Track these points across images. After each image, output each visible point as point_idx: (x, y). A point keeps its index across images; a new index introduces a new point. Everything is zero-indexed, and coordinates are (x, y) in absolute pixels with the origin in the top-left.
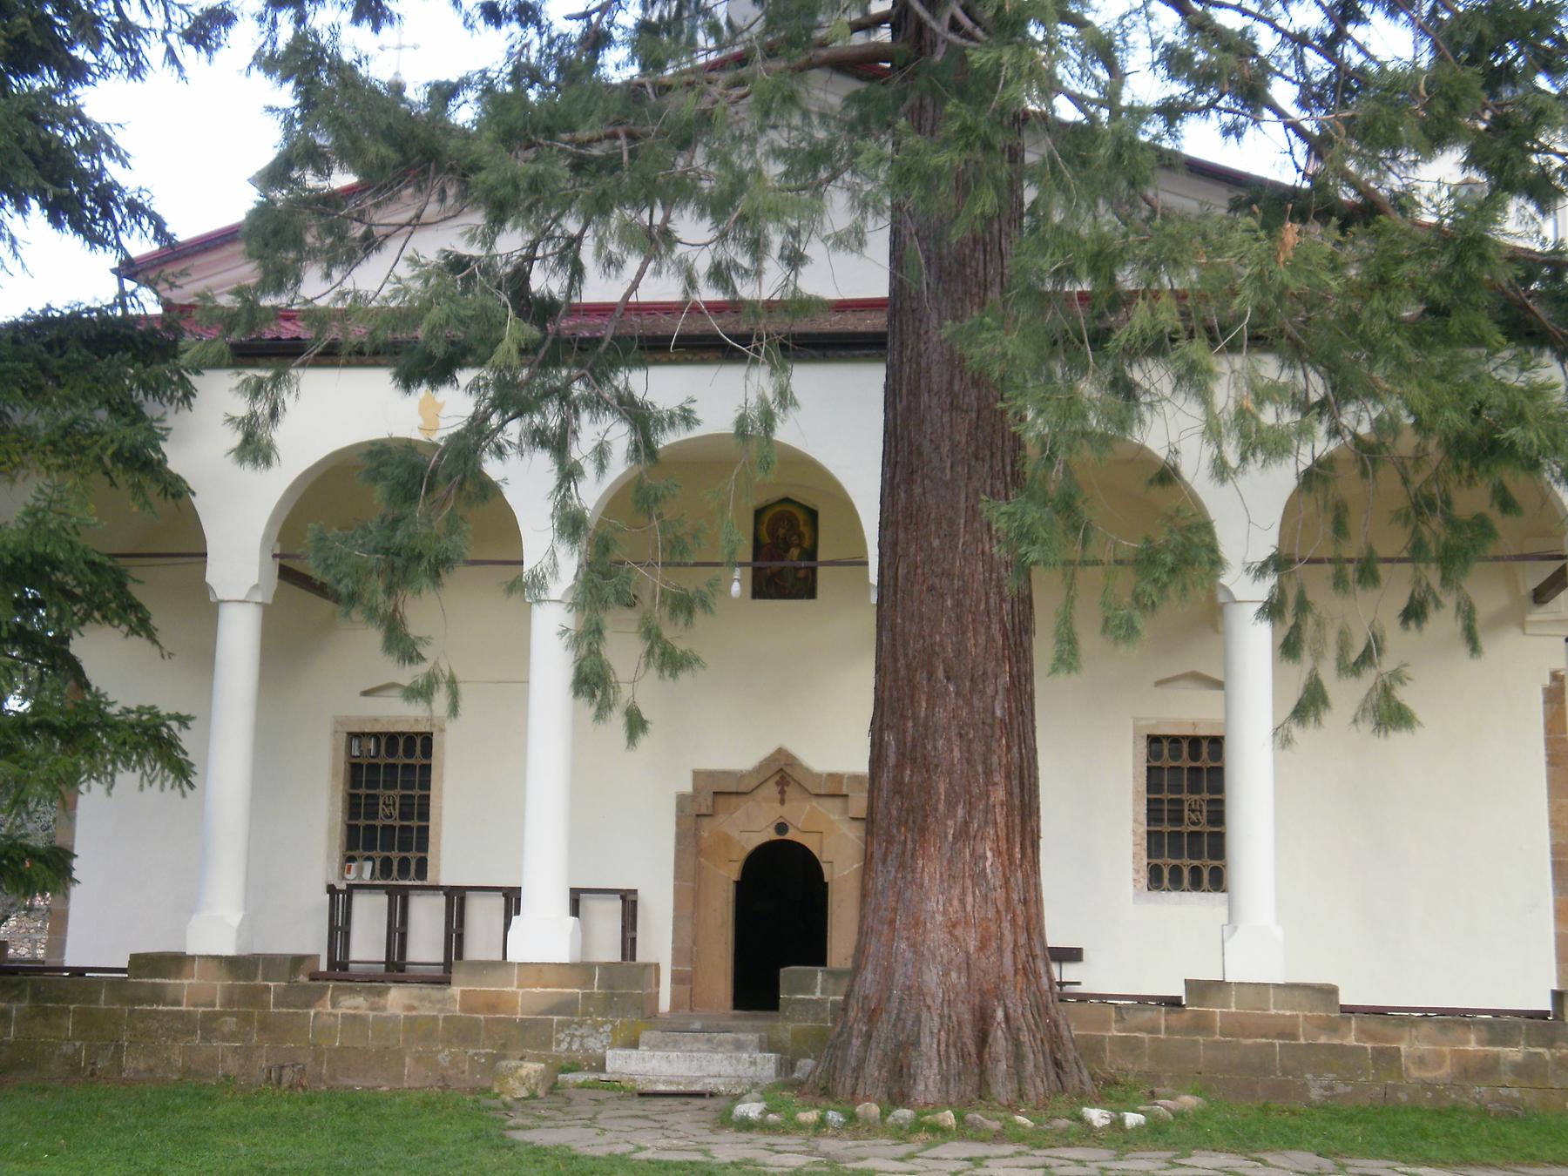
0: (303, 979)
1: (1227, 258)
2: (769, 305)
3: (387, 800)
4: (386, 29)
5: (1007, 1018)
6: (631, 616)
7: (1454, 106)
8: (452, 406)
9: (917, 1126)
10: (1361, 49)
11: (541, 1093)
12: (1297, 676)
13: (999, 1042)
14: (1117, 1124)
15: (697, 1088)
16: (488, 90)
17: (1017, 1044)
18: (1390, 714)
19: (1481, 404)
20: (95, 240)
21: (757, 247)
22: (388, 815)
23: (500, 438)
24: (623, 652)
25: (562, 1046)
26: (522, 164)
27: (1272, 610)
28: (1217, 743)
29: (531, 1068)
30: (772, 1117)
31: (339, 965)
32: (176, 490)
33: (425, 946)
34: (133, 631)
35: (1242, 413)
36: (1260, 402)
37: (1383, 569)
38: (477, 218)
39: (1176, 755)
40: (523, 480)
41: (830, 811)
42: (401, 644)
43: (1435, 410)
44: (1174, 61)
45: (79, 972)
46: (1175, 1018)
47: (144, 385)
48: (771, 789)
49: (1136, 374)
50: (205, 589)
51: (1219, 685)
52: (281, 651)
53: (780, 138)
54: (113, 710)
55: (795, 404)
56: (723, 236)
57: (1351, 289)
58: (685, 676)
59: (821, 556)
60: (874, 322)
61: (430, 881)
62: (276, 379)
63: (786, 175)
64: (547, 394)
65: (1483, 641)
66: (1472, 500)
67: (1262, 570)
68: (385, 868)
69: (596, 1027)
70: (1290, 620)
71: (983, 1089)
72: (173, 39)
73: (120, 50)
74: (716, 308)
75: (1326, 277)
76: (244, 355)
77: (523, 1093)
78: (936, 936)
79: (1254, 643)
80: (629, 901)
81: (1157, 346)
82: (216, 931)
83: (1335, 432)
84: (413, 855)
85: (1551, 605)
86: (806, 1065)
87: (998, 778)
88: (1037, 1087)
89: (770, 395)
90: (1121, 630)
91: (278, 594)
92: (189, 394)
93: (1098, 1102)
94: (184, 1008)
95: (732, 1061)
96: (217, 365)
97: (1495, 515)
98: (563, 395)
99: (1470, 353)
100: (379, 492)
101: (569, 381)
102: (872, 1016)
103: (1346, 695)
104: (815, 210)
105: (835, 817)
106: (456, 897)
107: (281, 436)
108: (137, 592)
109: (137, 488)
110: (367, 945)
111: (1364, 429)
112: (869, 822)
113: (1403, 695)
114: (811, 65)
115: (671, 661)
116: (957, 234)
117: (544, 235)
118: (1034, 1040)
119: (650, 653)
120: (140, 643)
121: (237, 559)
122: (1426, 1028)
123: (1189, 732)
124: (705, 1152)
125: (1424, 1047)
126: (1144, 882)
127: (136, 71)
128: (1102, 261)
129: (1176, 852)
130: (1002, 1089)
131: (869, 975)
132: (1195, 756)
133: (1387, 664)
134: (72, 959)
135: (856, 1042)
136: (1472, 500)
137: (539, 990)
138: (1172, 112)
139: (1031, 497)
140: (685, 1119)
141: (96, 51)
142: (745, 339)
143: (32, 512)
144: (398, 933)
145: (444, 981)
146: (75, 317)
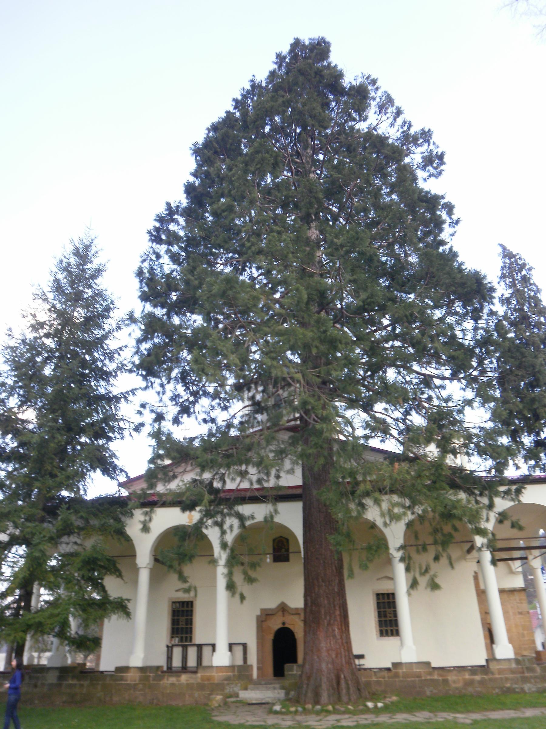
0: (159, 673)
1: (382, 472)
2: (271, 488)
3: (182, 620)
4: (180, 426)
5: (345, 677)
6: (241, 568)
7: (431, 434)
8: (195, 516)
9: (322, 711)
10: (411, 421)
11: (222, 705)
12: (411, 575)
13: (343, 685)
14: (376, 707)
15: (264, 701)
16: (202, 439)
17: (347, 684)
18: (434, 586)
19: (446, 505)
20: (112, 478)
21: (268, 474)
22: (182, 625)
23: (206, 524)
24: (238, 578)
25: (228, 690)
26: (209, 457)
27: (402, 559)
28: (393, 594)
29: (219, 697)
30: (283, 710)
31: (170, 668)
32: (128, 540)
33: (192, 662)
34: (118, 577)
35: (389, 510)
36: (393, 507)
37: (428, 547)
38: (198, 470)
39: (384, 598)
40: (213, 534)
41: (296, 618)
42: (183, 578)
43: (435, 507)
44: (367, 425)
45: (102, 672)
46: (390, 674)
47: (122, 513)
48: (280, 613)
49: (364, 501)
50: (135, 565)
51: (392, 579)
52: (156, 579)
53: (273, 448)
54: (111, 598)
55: (279, 513)
56: (259, 472)
57: (413, 478)
58: (254, 584)
59: (291, 550)
60: (299, 491)
61: (193, 642)
62: (151, 511)
63: (274, 456)
64: (218, 513)
65: (455, 565)
66: (447, 529)
67: (399, 549)
68: (181, 640)
69: (236, 684)
70: (407, 562)
71: (339, 699)
72: (131, 430)
73: (119, 433)
74: (257, 489)
75: (406, 476)
76: (143, 505)
77: (217, 705)
78: (324, 654)
79: (400, 568)
80: (245, 646)
81: (367, 494)
82: (137, 660)
83: (413, 513)
84: (188, 635)
85: (472, 554)
86: (292, 693)
87: (337, 608)
88: (354, 697)
89: (272, 511)
90: (364, 567)
91: (154, 566)
92: (132, 515)
93: (371, 700)
94: (129, 682)
95: (271, 693)
96: (137, 508)
97: (453, 532)
98: (222, 513)
99: (442, 492)
100: (176, 539)
101: (223, 509)
102: (309, 678)
103: (423, 581)
104: (282, 464)
105: (297, 620)
106: (200, 647)
107: (152, 525)
108: (119, 566)
109: (119, 539)
110: (177, 662)
111: (420, 512)
112: (305, 621)
113: (437, 580)
114: (280, 430)
115: (250, 580)
116: (316, 469)
117: (217, 473)
118: (353, 685)
119: (245, 578)
120: (119, 580)
121: (144, 556)
122: (455, 672)
123: (386, 592)
124: (265, 722)
125: (454, 678)
126: (379, 634)
127: (122, 438)
128: (352, 474)
129: (386, 626)
130: (345, 698)
131: (307, 666)
132: (388, 598)
133: (432, 572)
134: (102, 668)
135: (305, 686)
136: (447, 529)
137: (221, 674)
138: (366, 437)
139: (339, 534)
140: (260, 711)
141: (113, 434)
142: (265, 497)
143: (93, 546)
144: (185, 658)
145: (195, 672)
146: (107, 497)
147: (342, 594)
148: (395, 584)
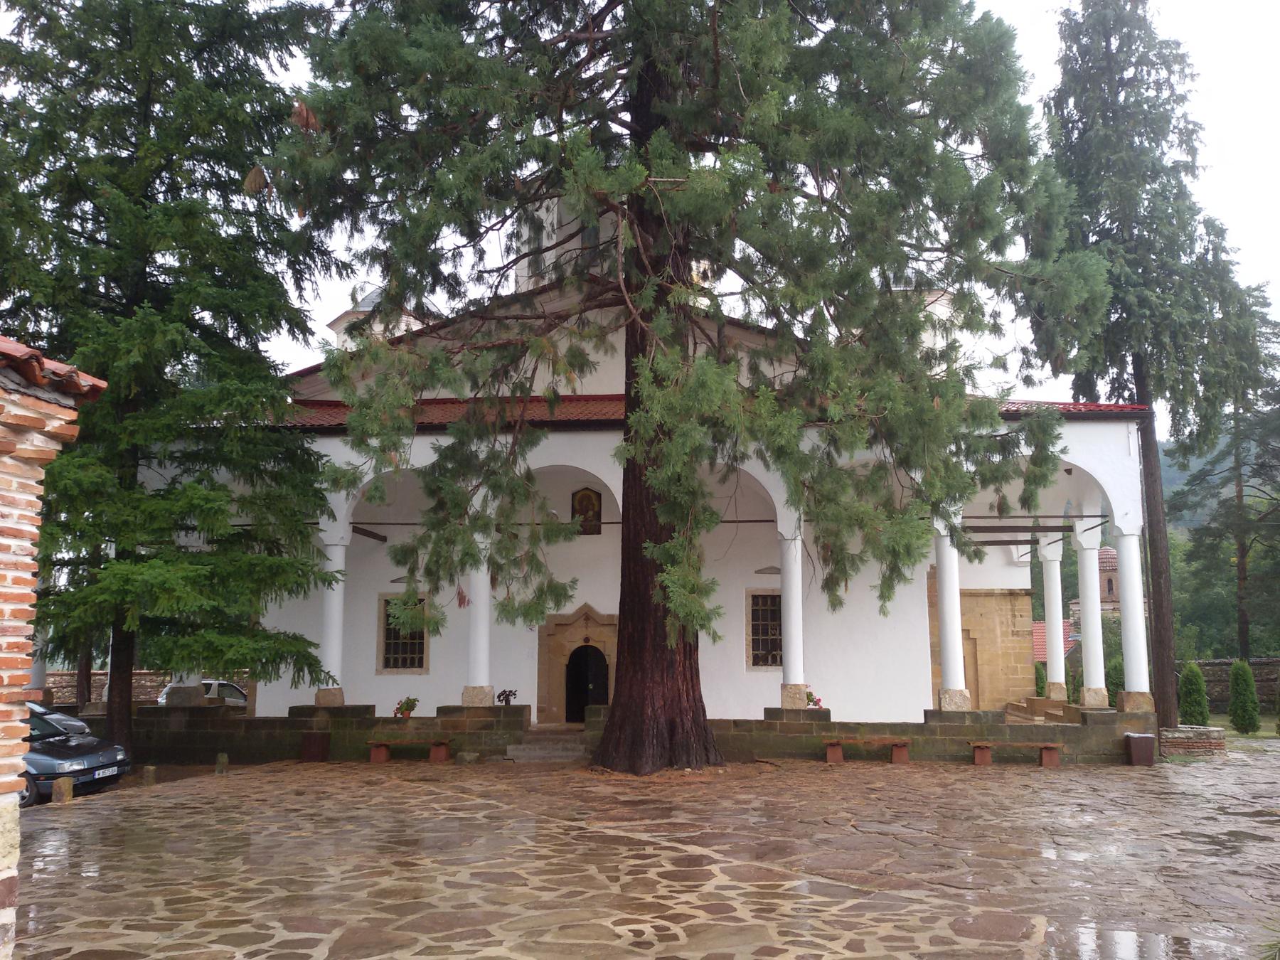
41: (606, 630)
48: (582, 622)
84: (416, 656)
147: (475, 688)
148: (782, 582)
